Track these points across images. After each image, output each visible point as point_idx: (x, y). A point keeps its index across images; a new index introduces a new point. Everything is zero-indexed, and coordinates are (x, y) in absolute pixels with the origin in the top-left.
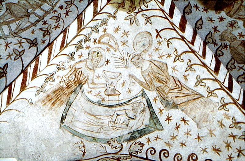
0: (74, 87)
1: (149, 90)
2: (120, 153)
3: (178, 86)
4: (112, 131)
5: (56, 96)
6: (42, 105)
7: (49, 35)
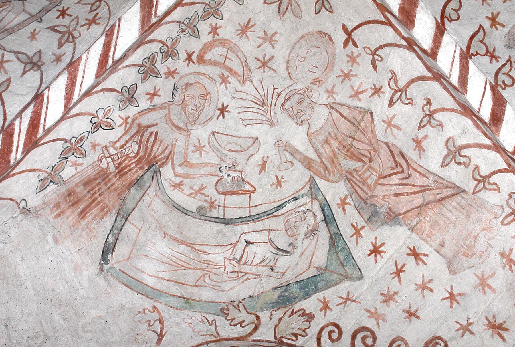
0: (136, 172)
1: (328, 180)
2: (252, 338)
3: (401, 167)
4: (233, 283)
5: (89, 195)
6: (53, 215)
7: (74, 41)
